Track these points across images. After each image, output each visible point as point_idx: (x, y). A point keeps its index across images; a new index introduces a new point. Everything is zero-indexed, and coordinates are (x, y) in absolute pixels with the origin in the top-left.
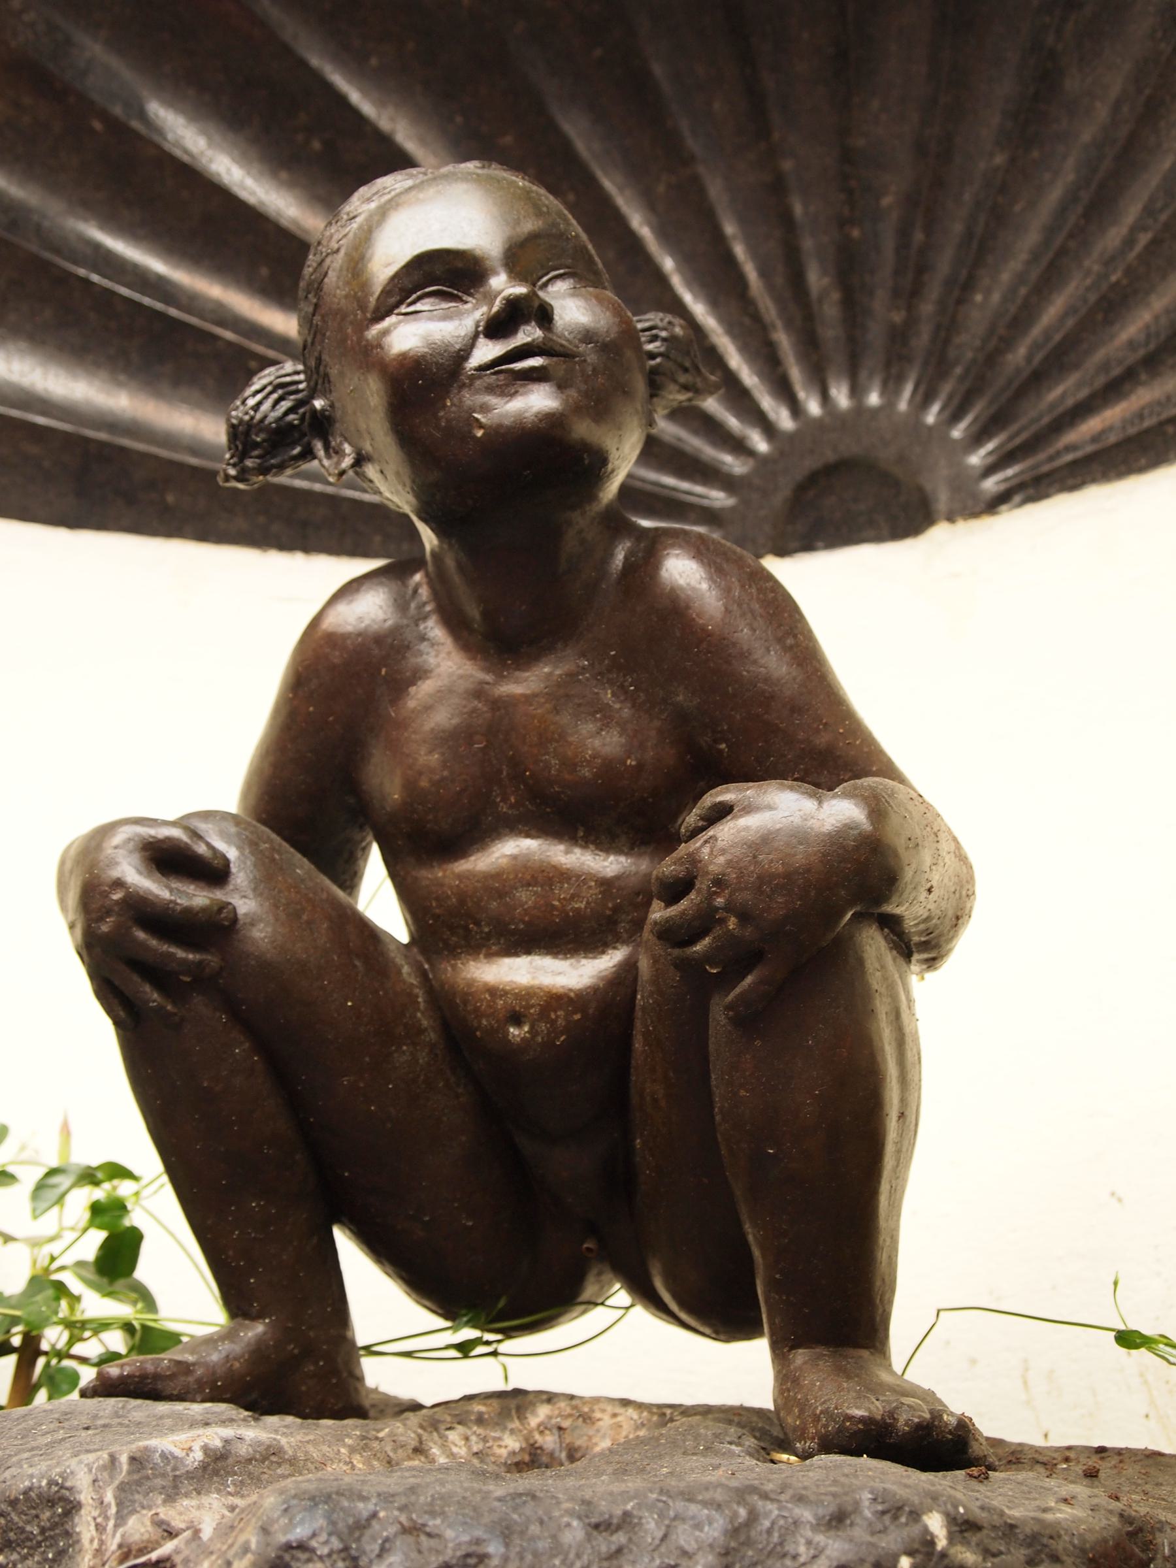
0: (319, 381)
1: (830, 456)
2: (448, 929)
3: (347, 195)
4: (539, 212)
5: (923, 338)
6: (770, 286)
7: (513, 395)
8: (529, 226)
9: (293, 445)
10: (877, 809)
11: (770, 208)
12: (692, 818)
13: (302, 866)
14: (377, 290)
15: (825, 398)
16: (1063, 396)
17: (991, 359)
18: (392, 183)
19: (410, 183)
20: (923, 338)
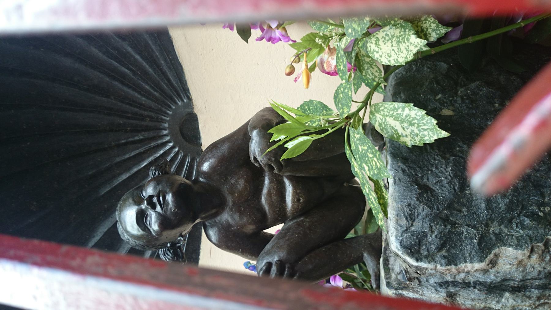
0: (163, 245)
1: (179, 134)
2: (281, 217)
3: (122, 240)
4: (128, 198)
5: (153, 115)
6: (141, 147)
7: (168, 203)
8: (131, 201)
9: (177, 251)
10: (254, 128)
11: (123, 147)
12: (257, 165)
13: (268, 247)
14: (144, 233)
15: (166, 135)
16: (165, 83)
17: (156, 100)
18: (120, 230)
19: (121, 227)
20: (153, 115)
